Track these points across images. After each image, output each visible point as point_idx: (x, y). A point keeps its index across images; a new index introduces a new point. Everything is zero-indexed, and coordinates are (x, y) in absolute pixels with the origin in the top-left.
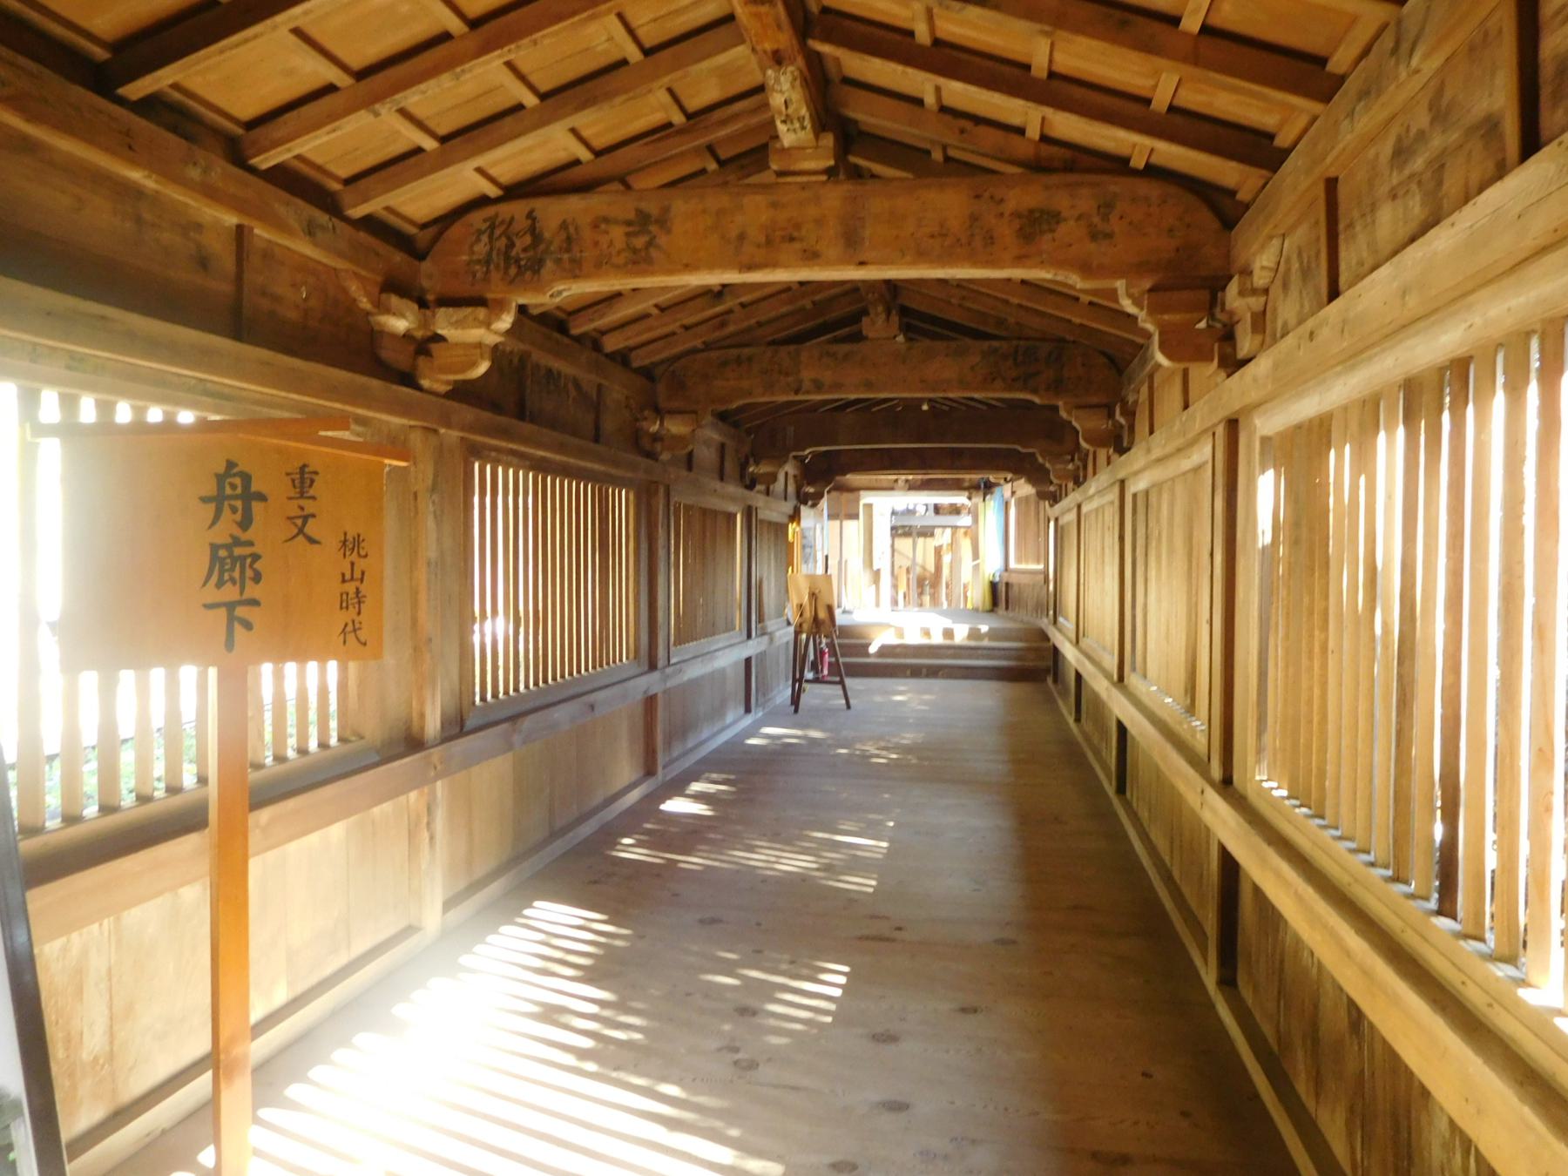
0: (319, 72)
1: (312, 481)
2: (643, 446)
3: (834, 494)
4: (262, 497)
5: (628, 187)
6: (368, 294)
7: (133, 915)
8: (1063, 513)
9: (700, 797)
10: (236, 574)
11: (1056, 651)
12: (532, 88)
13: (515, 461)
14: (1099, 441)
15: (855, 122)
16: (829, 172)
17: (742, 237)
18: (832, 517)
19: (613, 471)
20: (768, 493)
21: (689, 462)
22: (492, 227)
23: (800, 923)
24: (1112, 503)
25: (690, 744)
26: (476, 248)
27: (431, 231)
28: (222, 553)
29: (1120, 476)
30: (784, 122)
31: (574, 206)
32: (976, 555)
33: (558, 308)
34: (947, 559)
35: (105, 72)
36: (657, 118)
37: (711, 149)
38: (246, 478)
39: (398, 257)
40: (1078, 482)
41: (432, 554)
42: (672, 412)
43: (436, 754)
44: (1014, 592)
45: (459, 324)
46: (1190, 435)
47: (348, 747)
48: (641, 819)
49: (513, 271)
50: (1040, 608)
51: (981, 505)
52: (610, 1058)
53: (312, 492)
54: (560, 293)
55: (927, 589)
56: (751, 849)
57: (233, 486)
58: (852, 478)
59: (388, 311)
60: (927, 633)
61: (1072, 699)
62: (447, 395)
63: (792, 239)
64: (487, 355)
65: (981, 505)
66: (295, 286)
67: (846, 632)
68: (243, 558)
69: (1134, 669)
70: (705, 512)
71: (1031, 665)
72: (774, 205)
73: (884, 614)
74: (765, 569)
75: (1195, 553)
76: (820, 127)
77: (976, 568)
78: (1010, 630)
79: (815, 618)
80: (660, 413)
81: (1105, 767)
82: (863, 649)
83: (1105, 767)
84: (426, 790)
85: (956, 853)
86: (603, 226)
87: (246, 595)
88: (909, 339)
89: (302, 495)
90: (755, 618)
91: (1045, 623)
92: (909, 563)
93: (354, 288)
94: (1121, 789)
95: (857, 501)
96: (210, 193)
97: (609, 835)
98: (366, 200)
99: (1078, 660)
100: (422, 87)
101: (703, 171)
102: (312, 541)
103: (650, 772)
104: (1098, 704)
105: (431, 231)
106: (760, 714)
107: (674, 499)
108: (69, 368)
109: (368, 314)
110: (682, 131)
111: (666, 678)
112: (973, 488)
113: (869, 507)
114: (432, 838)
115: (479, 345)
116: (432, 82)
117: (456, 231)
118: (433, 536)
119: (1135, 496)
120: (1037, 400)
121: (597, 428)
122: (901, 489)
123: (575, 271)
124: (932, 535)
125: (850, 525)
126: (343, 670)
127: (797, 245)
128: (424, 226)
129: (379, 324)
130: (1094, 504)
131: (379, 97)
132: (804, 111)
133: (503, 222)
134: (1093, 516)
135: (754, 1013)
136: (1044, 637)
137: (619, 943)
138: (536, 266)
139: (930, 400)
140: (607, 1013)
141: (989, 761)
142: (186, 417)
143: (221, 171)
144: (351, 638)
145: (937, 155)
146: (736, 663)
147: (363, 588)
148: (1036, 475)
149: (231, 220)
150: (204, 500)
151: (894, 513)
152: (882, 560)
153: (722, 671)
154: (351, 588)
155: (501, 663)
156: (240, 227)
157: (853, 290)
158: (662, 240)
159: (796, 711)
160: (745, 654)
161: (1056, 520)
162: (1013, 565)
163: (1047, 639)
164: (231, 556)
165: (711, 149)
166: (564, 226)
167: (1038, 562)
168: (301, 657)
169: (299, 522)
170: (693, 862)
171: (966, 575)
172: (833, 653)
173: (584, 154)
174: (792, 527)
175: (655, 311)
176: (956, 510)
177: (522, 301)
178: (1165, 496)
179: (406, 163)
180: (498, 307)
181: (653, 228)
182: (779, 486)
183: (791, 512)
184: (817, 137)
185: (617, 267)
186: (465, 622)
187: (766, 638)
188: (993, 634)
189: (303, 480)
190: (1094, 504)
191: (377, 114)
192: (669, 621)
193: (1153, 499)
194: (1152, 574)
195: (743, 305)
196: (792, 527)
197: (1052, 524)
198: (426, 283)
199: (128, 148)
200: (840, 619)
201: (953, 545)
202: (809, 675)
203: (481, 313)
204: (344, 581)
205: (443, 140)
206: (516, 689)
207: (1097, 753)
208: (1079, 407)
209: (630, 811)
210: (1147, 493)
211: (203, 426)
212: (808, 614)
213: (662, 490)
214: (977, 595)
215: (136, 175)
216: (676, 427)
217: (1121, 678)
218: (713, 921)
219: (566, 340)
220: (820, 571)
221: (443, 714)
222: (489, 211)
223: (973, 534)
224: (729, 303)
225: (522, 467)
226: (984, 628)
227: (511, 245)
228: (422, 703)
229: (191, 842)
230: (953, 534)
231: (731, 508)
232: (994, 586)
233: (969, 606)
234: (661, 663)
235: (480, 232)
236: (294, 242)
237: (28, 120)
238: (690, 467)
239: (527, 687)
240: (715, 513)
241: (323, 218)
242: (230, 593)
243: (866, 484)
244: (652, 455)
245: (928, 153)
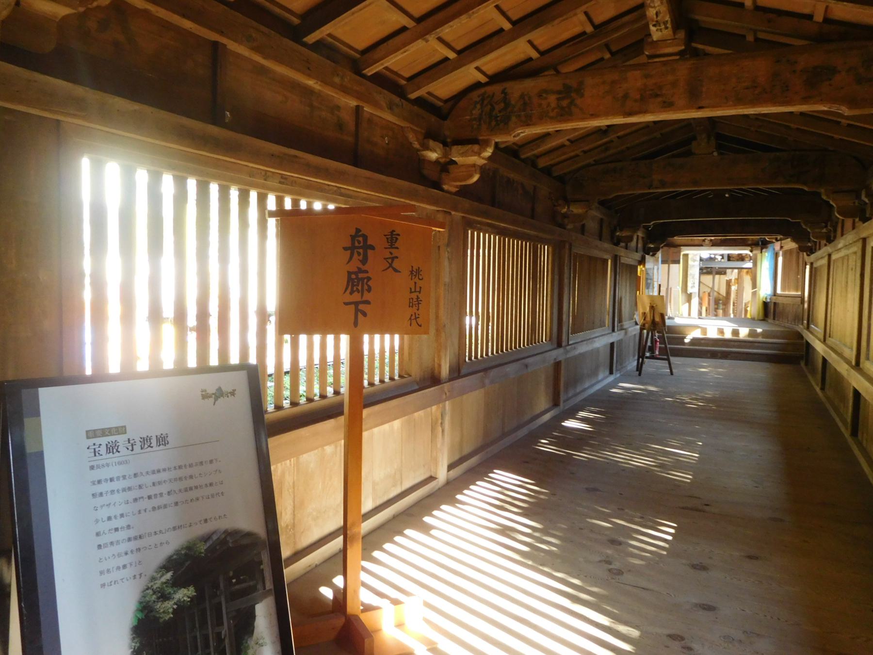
0: (398, 20)
1: (397, 239)
2: (557, 220)
3: (665, 248)
4: (372, 248)
5: (558, 72)
6: (418, 140)
7: (305, 458)
8: (818, 259)
9: (584, 420)
10: (360, 288)
11: (808, 345)
12: (508, 19)
13: (490, 230)
14: (846, 213)
15: (697, 21)
16: (681, 53)
17: (626, 96)
18: (663, 262)
19: (541, 235)
20: (626, 248)
21: (583, 230)
22: (483, 100)
23: (649, 496)
24: (855, 253)
25: (578, 389)
26: (474, 112)
27: (450, 104)
28: (353, 276)
29: (864, 235)
30: (654, 25)
31: (529, 85)
32: (754, 285)
33: (514, 144)
34: (734, 288)
35: (295, 30)
36: (578, 30)
37: (607, 46)
38: (365, 238)
39: (433, 119)
40: (830, 240)
41: (447, 280)
42: (575, 201)
43: (446, 386)
45: (464, 154)
47: (404, 380)
48: (553, 429)
49: (493, 123)
50: (798, 319)
51: (759, 255)
52: (536, 558)
53: (396, 245)
54: (519, 134)
55: (721, 306)
56: (615, 451)
57: (359, 242)
58: (677, 239)
59: (427, 148)
61: (819, 376)
62: (457, 194)
63: (657, 96)
64: (478, 171)
65: (759, 255)
66: (383, 137)
67: (672, 330)
68: (363, 279)
70: (591, 258)
72: (647, 76)
74: (624, 292)
76: (676, 28)
77: (754, 294)
79: (653, 322)
80: (567, 202)
81: (844, 421)
84: (441, 405)
85: (745, 463)
86: (544, 95)
87: (364, 299)
88: (720, 154)
89: (392, 248)
90: (617, 321)
91: (800, 328)
92: (709, 290)
93: (411, 137)
95: (680, 252)
96: (344, 90)
97: (534, 437)
98: (419, 88)
99: (825, 352)
100: (451, 24)
101: (602, 59)
102: (396, 270)
103: (556, 404)
104: (839, 379)
105: (450, 104)
106: (618, 375)
107: (574, 250)
108: (280, 182)
109: (418, 150)
110: (592, 36)
111: (567, 352)
112: (753, 245)
113: (686, 256)
114: (443, 431)
115: (474, 165)
116: (456, 21)
117: (462, 103)
118: (447, 270)
120: (806, 189)
121: (533, 209)
122: (707, 245)
123: (528, 122)
124: (725, 273)
125: (674, 267)
126: (402, 340)
127: (660, 99)
128: (446, 101)
129: (423, 155)
130: (842, 253)
131: (428, 32)
132: (668, 18)
133: (488, 97)
134: (840, 264)
135: (620, 543)
136: (800, 336)
137: (542, 497)
138: (506, 120)
139: (729, 191)
140: (537, 534)
142: (331, 207)
143: (349, 77)
144: (414, 322)
145: (750, 38)
146: (605, 346)
147: (420, 296)
148: (800, 236)
149: (353, 103)
150: (345, 249)
151: (701, 260)
152: (693, 289)
154: (414, 296)
155: (473, 341)
156: (357, 107)
157: (687, 124)
158: (578, 101)
159: (640, 375)
160: (611, 341)
161: (812, 264)
162: (779, 291)
163: (802, 337)
164: (357, 278)
165: (607, 46)
166: (522, 96)
167: (797, 290)
168: (382, 332)
169: (390, 261)
170: (582, 456)
171: (747, 296)
172: (663, 341)
173: (534, 55)
174: (640, 268)
175: (567, 143)
176: (741, 258)
177: (497, 140)
179: (440, 67)
180: (484, 144)
181: (573, 95)
182: (633, 244)
183: (639, 259)
184: (674, 33)
185: (552, 118)
186: (462, 314)
188: (764, 334)
189: (392, 238)
190: (842, 253)
191: (427, 41)
192: (568, 320)
195: (619, 137)
196: (640, 268)
197: (808, 267)
198: (447, 133)
199: (308, 69)
200: (668, 322)
201: (739, 280)
202: (648, 354)
203: (476, 147)
204: (411, 292)
205: (459, 52)
206: (487, 354)
207: (837, 410)
209: (545, 425)
211: (338, 209)
212: (649, 319)
213: (567, 246)
214: (754, 310)
215: (311, 83)
216: (576, 210)
218: (595, 490)
219: (517, 161)
220: (656, 293)
221: (450, 366)
222: (482, 91)
223: (753, 274)
224: (612, 136)
225: (493, 233)
227: (493, 109)
228: (440, 360)
229: (330, 424)
230: (739, 273)
231: (606, 257)
232: (765, 305)
233: (749, 316)
234: (564, 344)
235: (476, 103)
236: (383, 113)
237: (264, 58)
239: (492, 353)
240: (596, 259)
241: (396, 99)
242: (356, 297)
244: (562, 226)
245: (744, 37)
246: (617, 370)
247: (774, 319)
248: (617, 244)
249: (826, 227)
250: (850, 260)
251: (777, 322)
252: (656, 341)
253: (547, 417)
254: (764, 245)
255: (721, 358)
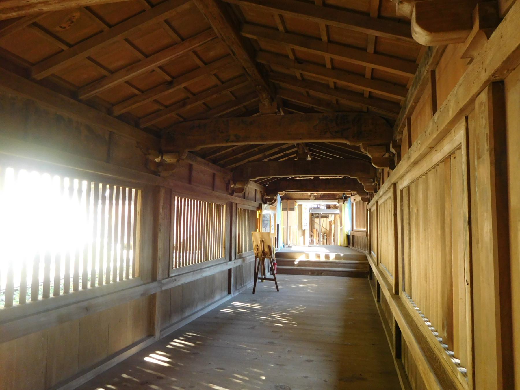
18: (283, 209)
24: (390, 197)
32: (341, 225)
34: (333, 226)
42: (168, 152)
44: (355, 239)
46: (442, 128)
60: (318, 256)
65: (343, 205)
69: (404, 290)
71: (360, 272)
73: (305, 249)
75: (447, 221)
77: (341, 229)
78: (352, 255)
80: (161, 153)
82: (292, 263)
83: (391, 335)
91: (367, 252)
94: (399, 355)
103: (150, 334)
106: (237, 294)
113: (301, 205)
119: (402, 191)
125: (290, 212)
136: (366, 258)
141: (331, 328)
146: (223, 272)
148: (360, 191)
152: (306, 226)
153: (212, 278)
162: (355, 228)
167: (364, 228)
174: (258, 213)
178: (421, 187)
183: (257, 206)
187: (240, 260)
188: (346, 257)
193: (413, 190)
194: (414, 236)
208: (370, 146)
210: (408, 187)
212: (260, 250)
214: (341, 240)
217: (397, 292)
226: (342, 255)
230: (335, 217)
232: (348, 237)
238: (190, 182)
243: (299, 197)
246: (236, 289)
247: (353, 246)
248: (232, 194)
249: (374, 182)
250: (388, 204)
251: (354, 248)
252: (274, 264)
253: (134, 350)
254: (345, 198)
255: (318, 275)
